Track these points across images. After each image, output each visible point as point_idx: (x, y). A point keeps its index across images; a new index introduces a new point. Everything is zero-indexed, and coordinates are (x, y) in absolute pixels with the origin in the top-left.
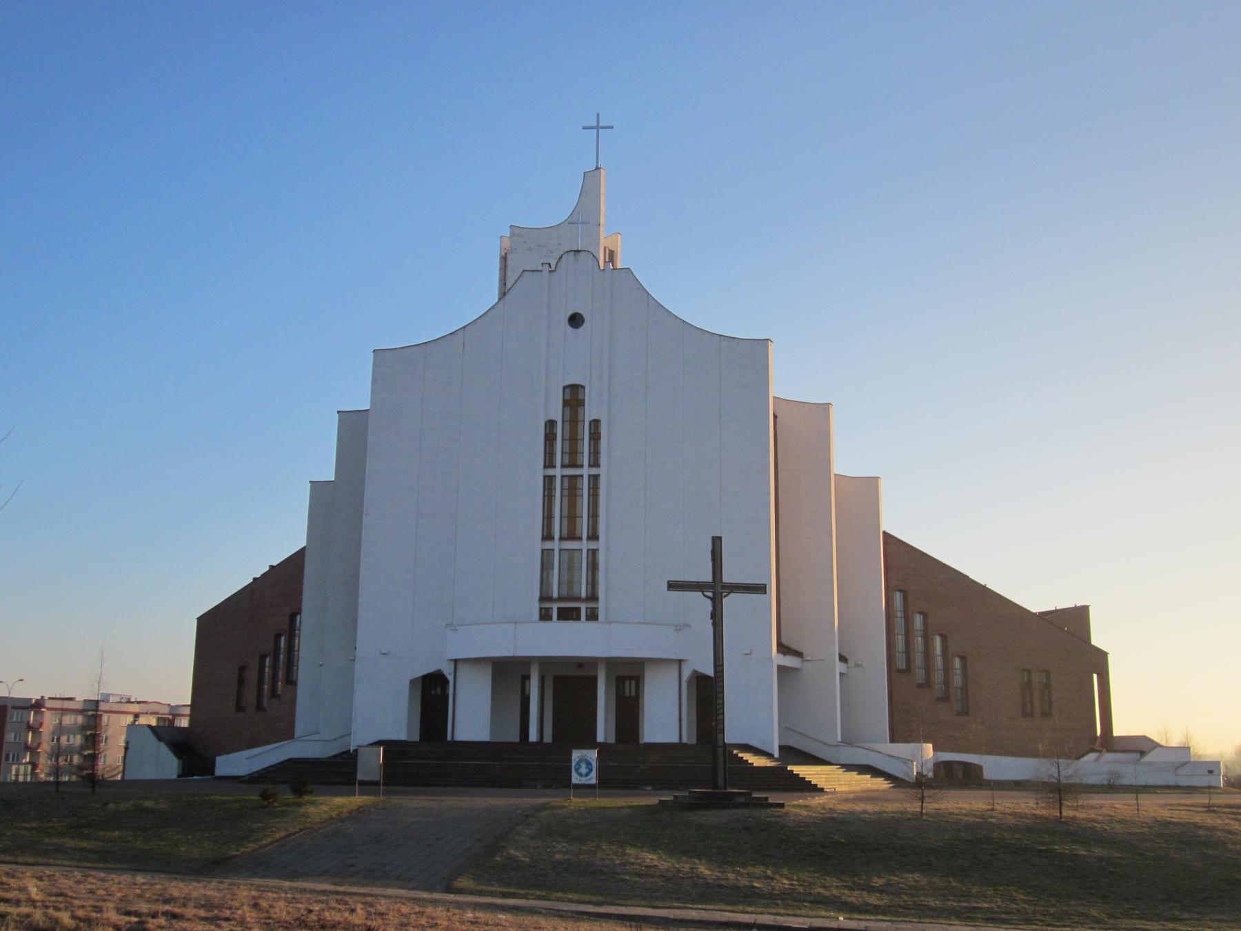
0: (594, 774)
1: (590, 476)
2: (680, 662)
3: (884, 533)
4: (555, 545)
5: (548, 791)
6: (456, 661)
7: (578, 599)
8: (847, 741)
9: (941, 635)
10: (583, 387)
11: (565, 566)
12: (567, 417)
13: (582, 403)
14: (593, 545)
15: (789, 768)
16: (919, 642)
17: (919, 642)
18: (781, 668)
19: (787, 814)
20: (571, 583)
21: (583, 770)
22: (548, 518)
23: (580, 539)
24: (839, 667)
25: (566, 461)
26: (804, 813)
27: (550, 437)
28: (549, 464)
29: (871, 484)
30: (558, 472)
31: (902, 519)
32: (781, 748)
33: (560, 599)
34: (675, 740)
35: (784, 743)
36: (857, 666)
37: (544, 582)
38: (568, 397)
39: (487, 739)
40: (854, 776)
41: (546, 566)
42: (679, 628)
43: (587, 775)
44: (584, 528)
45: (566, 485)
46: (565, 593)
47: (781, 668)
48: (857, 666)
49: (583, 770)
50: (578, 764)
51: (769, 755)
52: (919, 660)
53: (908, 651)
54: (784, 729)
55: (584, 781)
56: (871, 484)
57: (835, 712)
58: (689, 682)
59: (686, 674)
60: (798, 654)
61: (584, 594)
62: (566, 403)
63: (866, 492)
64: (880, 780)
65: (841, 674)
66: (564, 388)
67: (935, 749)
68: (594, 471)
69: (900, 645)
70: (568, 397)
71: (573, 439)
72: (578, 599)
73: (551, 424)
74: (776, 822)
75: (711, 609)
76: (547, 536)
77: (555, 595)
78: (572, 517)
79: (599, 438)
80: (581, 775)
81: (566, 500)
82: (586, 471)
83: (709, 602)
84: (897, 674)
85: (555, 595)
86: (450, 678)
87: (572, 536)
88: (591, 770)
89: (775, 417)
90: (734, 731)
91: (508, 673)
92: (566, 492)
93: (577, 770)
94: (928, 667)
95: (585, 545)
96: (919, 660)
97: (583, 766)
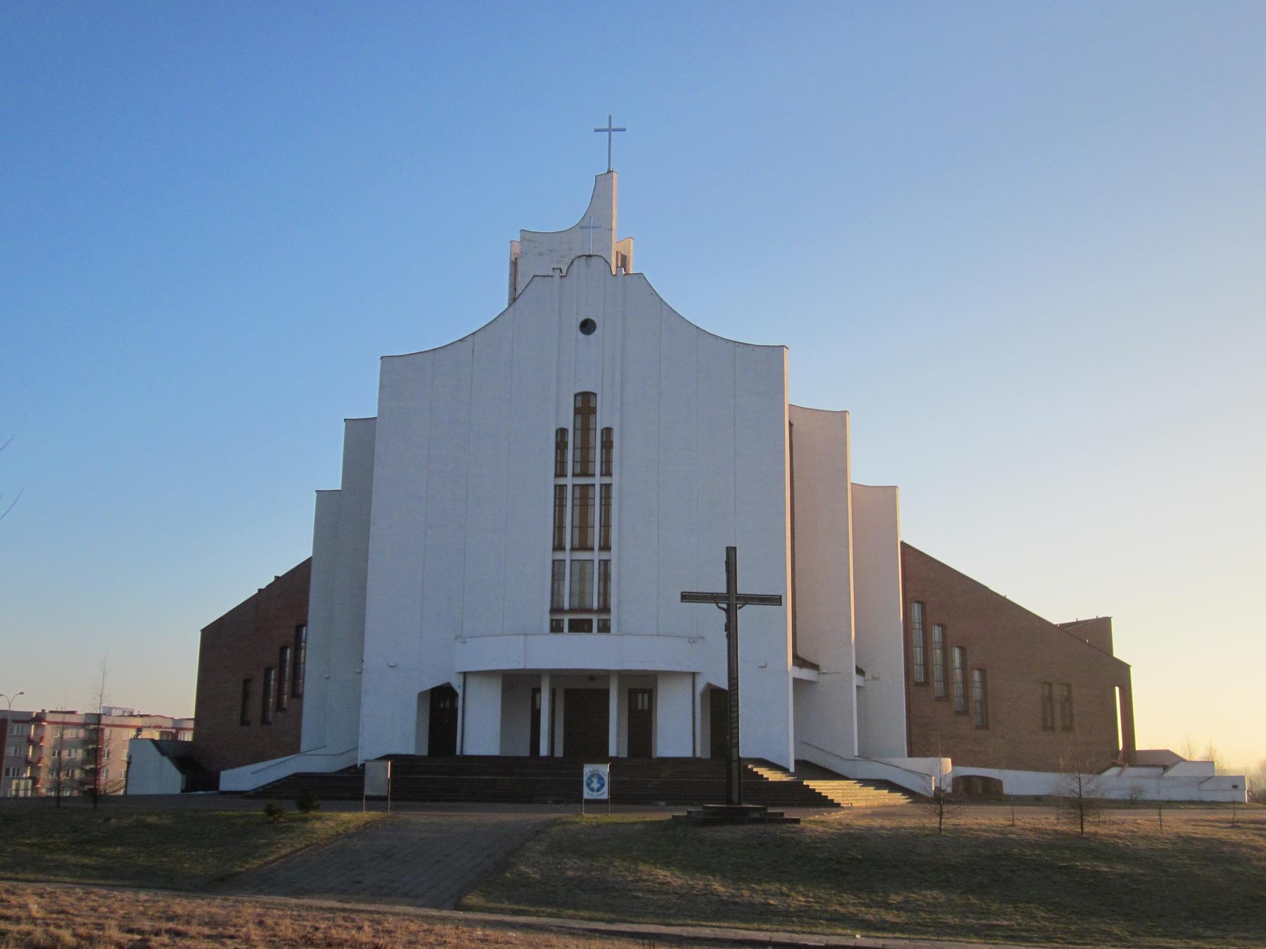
0: (606, 789)
1: (601, 485)
2: (694, 674)
3: (902, 543)
4: (566, 556)
5: (559, 806)
6: (465, 674)
7: (590, 611)
8: (864, 755)
9: (960, 648)
10: (595, 395)
11: (576, 577)
12: (579, 425)
13: (594, 411)
14: (604, 556)
15: (805, 783)
16: (937, 654)
17: (937, 654)
18: (797, 681)
19: (802, 830)
20: (582, 594)
21: (595, 785)
22: (559, 528)
23: (592, 549)
24: (856, 680)
25: (578, 470)
26: (821, 829)
27: (561, 446)
28: (560, 473)
29: (889, 493)
30: (569, 481)
31: (921, 529)
32: (797, 762)
33: (572, 610)
34: (689, 754)
35: (800, 758)
36: (874, 678)
37: (555, 593)
38: (579, 405)
39: (497, 753)
40: (871, 791)
41: (557, 577)
42: (692, 640)
43: (598, 790)
44: (596, 538)
45: (577, 495)
46: (576, 605)
47: (797, 681)
48: (874, 678)
49: (595, 785)
50: (590, 778)
51: (784, 770)
52: (937, 672)
53: (926, 663)
54: (800, 743)
55: (595, 796)
56: (889, 493)
57: (852, 726)
58: (703, 695)
59: (700, 687)
60: (815, 667)
61: (595, 606)
62: (577, 411)
63: (883, 501)
64: (898, 795)
65: (858, 687)
66: (576, 396)
67: (953, 764)
68: (606, 480)
69: (919, 658)
70: (579, 405)
71: (585, 448)
72: (590, 611)
73: (562, 432)
74: (792, 838)
75: (725, 620)
76: (558, 547)
77: (566, 606)
78: (583, 527)
79: (611, 447)
80: (592, 790)
81: (577, 510)
82: (597, 480)
83: (723, 614)
84: (915, 687)
85: (566, 606)
86: (460, 691)
87: (584, 546)
88: (603, 785)
89: (791, 425)
90: (749, 745)
91: (518, 686)
92: (577, 502)
93: (588, 785)
94: (947, 680)
95: (596, 556)
96: (937, 672)
97: (595, 780)
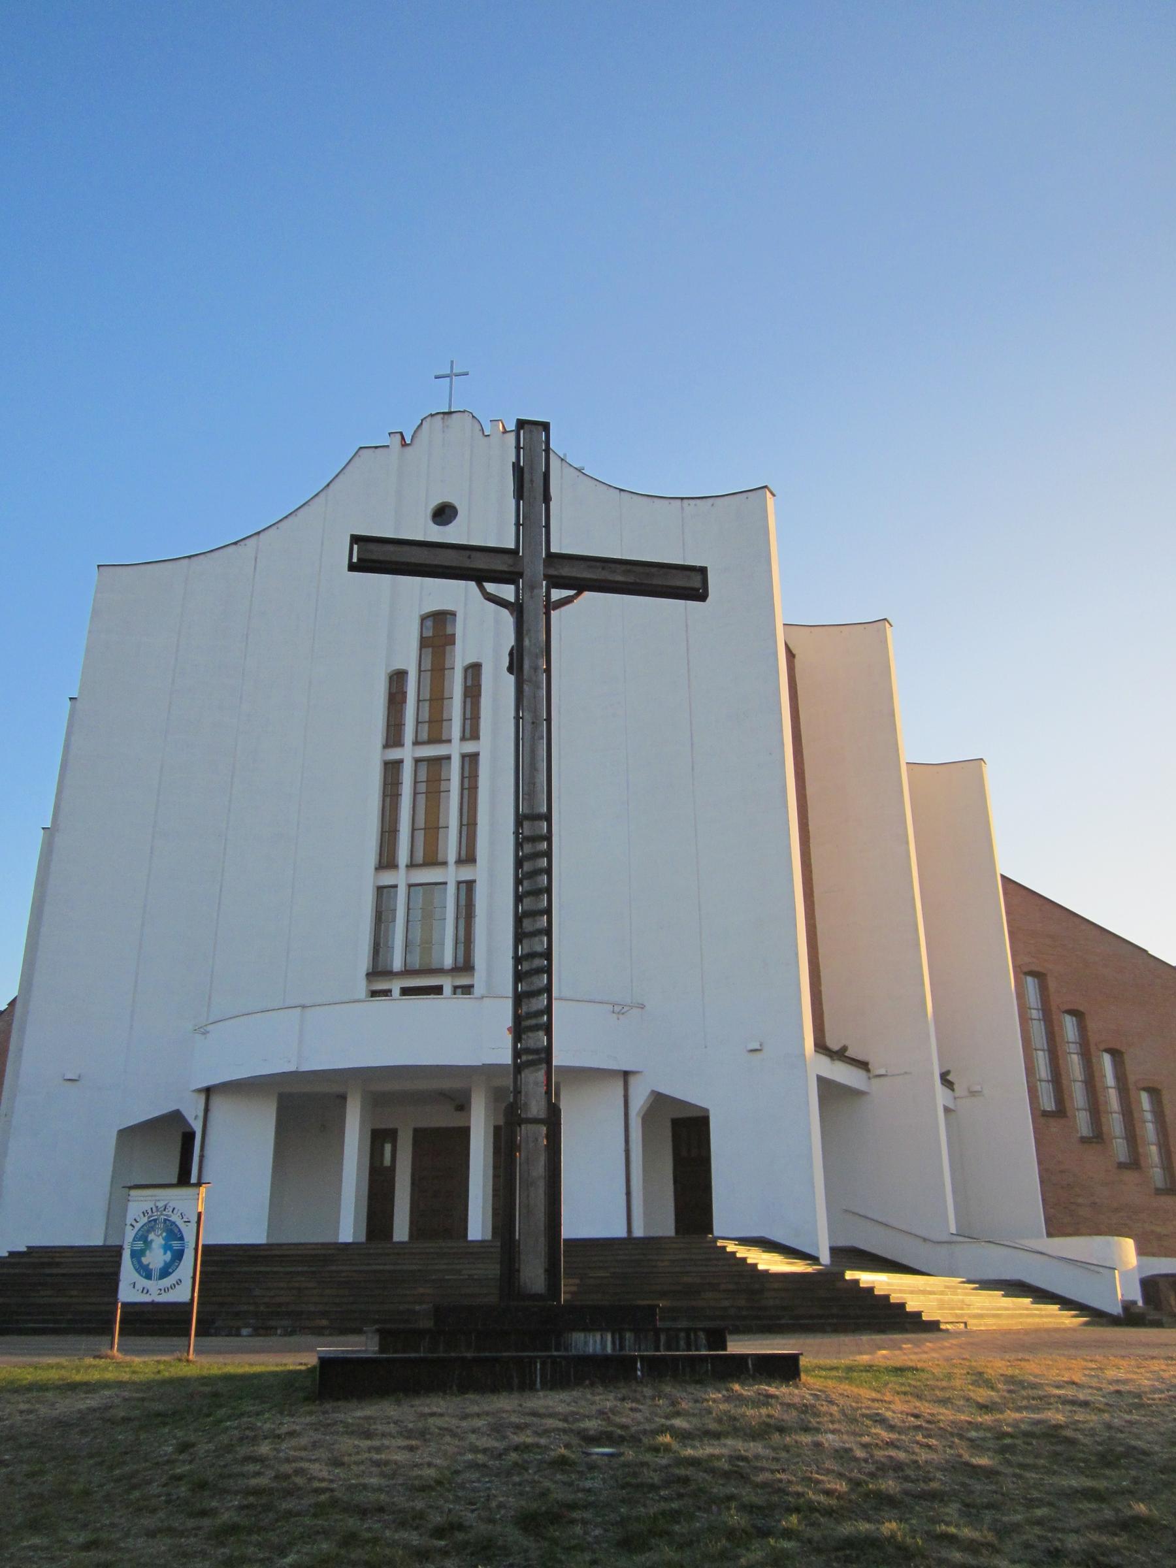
0: (187, 1269)
1: (463, 756)
2: (626, 1074)
3: (1003, 876)
4: (400, 878)
5: (294, 1339)
6: (208, 1091)
7: (440, 971)
8: (967, 1234)
9: (1109, 1051)
10: (453, 614)
11: (417, 914)
12: (427, 665)
13: (451, 640)
14: (466, 874)
15: (849, 1275)
16: (1074, 1063)
17: (1074, 1063)
18: (824, 1083)
19: (807, 1418)
20: (427, 945)
21: (156, 1257)
22: (388, 833)
23: (444, 864)
24: (941, 1095)
25: (424, 736)
26: (897, 1408)
27: (396, 699)
28: (393, 738)
29: (967, 776)
30: (407, 753)
31: (1031, 854)
32: (835, 1251)
33: (407, 972)
34: (620, 1232)
35: (842, 1243)
36: (973, 1093)
37: (379, 946)
38: (429, 633)
39: (262, 1240)
40: (996, 1300)
41: (382, 917)
42: (620, 1009)
43: (165, 1273)
44: (451, 847)
45: (423, 776)
46: (416, 962)
47: (824, 1083)
48: (973, 1093)
49: (156, 1257)
50: (143, 1238)
51: (814, 1259)
52: (1078, 1095)
53: (1057, 1079)
54: (839, 1211)
55: (154, 1292)
56: (967, 776)
57: (942, 1173)
58: (649, 1117)
59: (639, 1101)
60: (863, 1065)
61: (448, 962)
62: (424, 643)
63: (960, 789)
64: (1054, 1308)
65: (947, 1110)
66: (424, 618)
67: (1141, 1251)
68: (470, 747)
69: (1043, 1071)
70: (429, 633)
71: (437, 699)
72: (440, 971)
73: (398, 678)
74: (739, 1470)
75: (510, 641)
76: (386, 862)
77: (397, 965)
78: (432, 829)
79: (479, 695)
80: (147, 1273)
81: (422, 799)
82: (455, 749)
83: (507, 619)
84: (1050, 1117)
85: (397, 965)
86: (197, 1127)
87: (433, 860)
88: (178, 1255)
89: (790, 655)
90: (732, 1214)
91: (304, 1108)
92: (422, 787)
93: (136, 1255)
94: (1096, 1109)
95: (451, 875)
96: (1078, 1095)
97: (157, 1240)
